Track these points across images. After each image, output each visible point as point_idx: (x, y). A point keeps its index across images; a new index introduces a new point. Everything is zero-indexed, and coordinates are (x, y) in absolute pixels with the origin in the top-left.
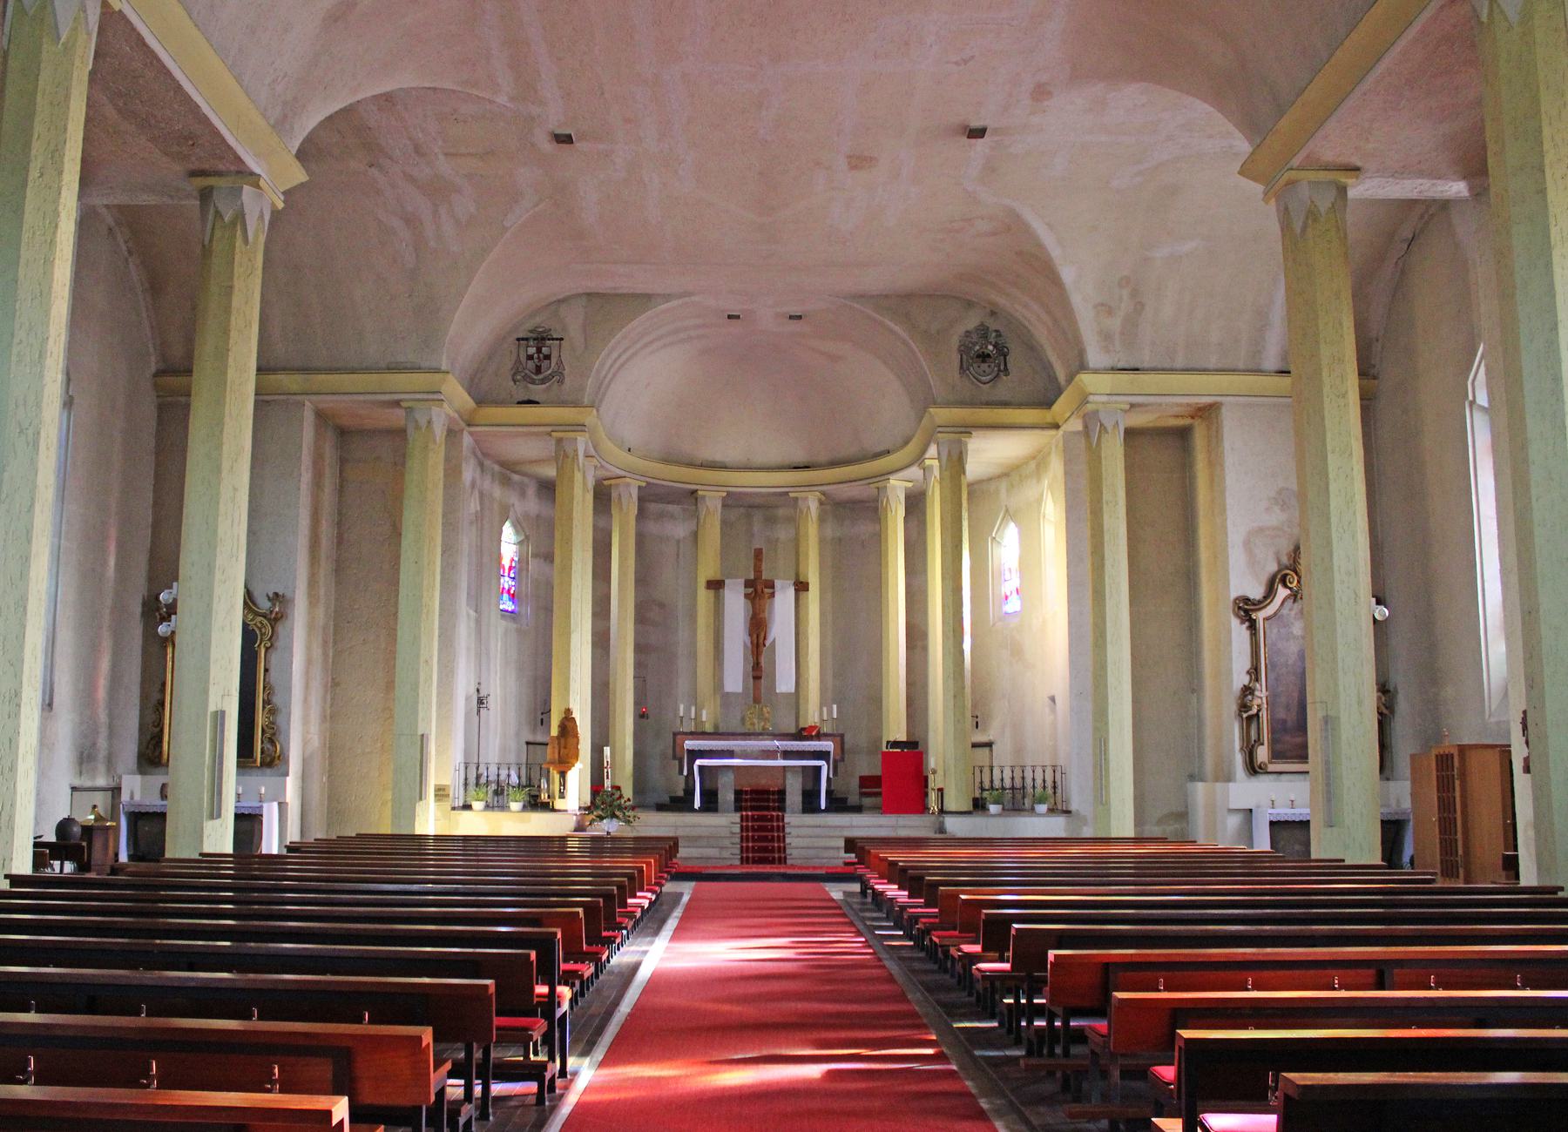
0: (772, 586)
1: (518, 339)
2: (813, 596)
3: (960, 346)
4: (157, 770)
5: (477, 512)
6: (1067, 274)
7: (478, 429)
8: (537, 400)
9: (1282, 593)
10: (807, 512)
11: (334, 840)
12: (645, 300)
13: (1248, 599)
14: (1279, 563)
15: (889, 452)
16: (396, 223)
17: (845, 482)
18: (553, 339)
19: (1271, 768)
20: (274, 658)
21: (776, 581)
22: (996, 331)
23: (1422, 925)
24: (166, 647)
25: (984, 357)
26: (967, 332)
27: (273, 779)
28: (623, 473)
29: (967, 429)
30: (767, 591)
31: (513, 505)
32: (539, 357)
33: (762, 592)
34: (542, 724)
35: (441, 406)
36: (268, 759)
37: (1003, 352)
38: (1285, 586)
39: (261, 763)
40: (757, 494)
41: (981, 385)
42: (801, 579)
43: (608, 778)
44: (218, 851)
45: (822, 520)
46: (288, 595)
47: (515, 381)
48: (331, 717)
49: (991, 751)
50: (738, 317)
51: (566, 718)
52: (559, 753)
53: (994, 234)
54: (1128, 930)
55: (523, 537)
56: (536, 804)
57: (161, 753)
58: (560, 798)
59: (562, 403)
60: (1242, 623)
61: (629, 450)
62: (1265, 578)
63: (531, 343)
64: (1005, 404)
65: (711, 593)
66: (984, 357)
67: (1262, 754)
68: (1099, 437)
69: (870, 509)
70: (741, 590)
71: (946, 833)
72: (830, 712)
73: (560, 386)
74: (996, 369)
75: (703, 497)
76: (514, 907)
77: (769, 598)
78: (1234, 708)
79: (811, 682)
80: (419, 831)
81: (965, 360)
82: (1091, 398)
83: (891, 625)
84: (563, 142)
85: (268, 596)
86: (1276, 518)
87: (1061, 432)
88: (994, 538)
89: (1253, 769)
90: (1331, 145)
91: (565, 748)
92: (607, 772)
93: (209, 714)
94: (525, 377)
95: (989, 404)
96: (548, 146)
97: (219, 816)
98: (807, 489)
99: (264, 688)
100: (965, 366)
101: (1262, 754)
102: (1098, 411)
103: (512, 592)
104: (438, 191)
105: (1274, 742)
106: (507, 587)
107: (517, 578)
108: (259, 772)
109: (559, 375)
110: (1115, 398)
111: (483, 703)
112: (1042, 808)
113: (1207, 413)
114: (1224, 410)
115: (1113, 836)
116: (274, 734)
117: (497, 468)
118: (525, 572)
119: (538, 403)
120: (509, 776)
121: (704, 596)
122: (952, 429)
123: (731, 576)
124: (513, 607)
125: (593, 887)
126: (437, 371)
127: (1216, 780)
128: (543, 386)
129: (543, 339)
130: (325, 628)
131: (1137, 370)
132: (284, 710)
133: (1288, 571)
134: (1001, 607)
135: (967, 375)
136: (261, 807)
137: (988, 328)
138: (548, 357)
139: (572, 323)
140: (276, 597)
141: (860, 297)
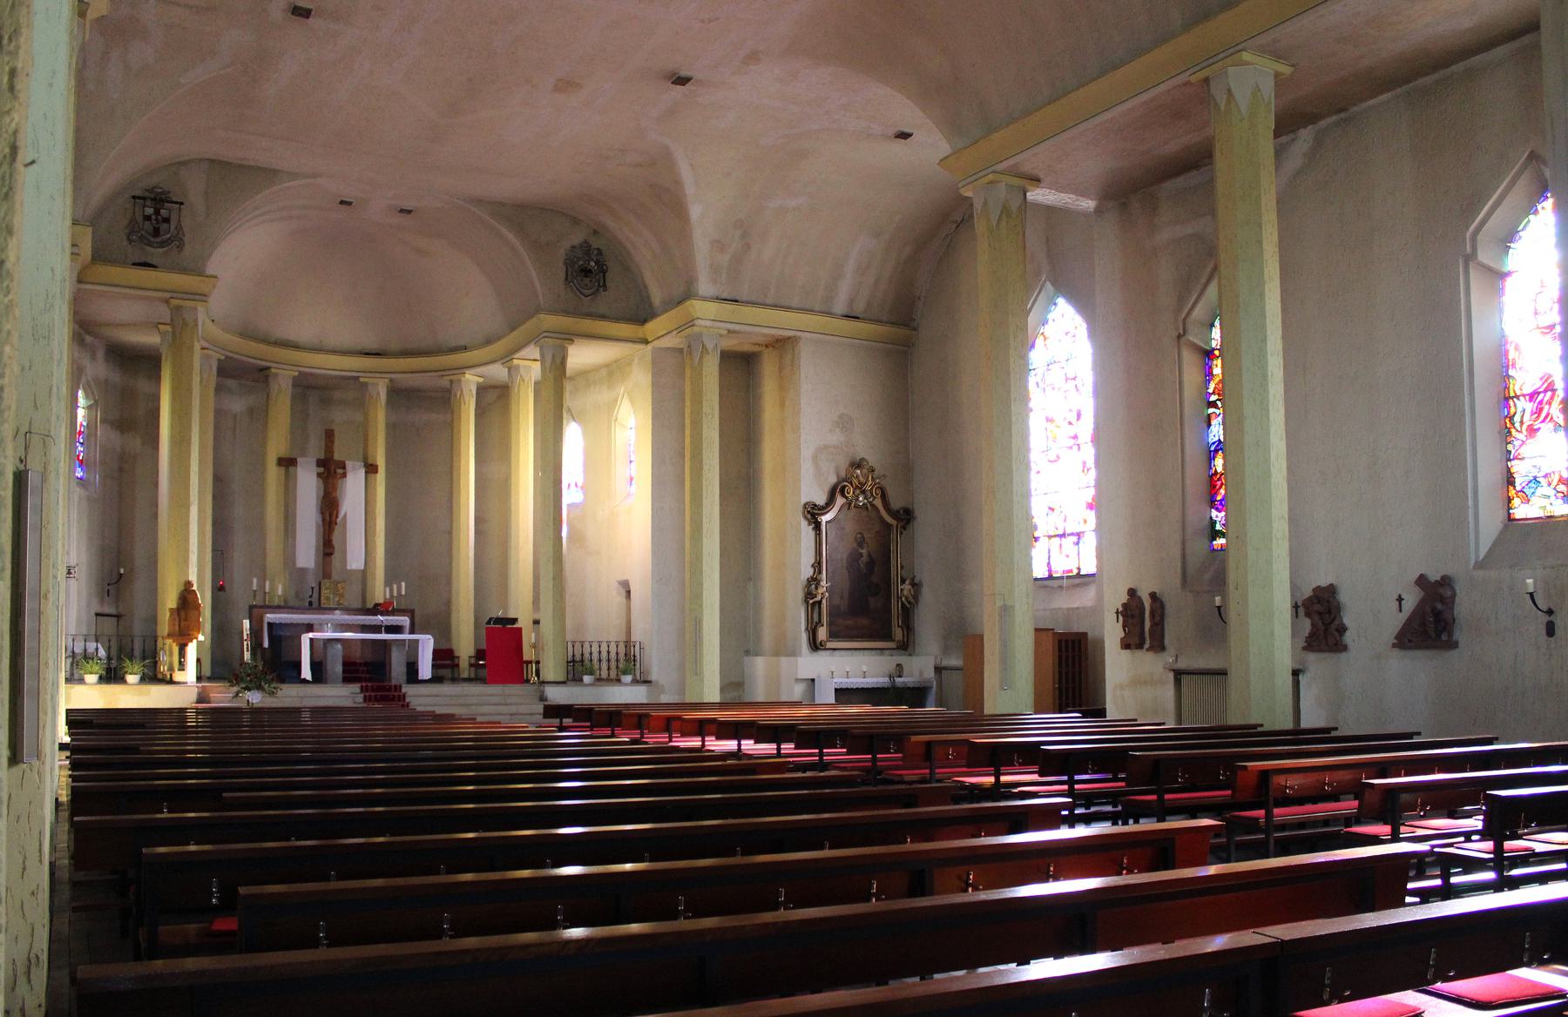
0: (344, 467)
1: (134, 197)
2: (381, 477)
3: (566, 260)
6: (695, 211)
7: (89, 287)
8: (154, 263)
9: (840, 501)
12: (269, 175)
13: (815, 505)
14: (838, 475)
15: (466, 349)
17: (418, 372)
18: (173, 202)
19: (829, 645)
21: (347, 462)
22: (599, 249)
25: (586, 272)
26: (573, 247)
29: (570, 336)
30: (340, 471)
33: (335, 472)
34: (108, 595)
38: (843, 495)
41: (583, 297)
42: (370, 461)
47: (130, 241)
50: (350, 204)
51: (186, 590)
52: (180, 625)
53: (639, 165)
55: (92, 402)
56: (153, 676)
58: (179, 670)
59: (183, 270)
60: (809, 524)
62: (827, 488)
63: (148, 203)
64: (603, 317)
65: (283, 470)
66: (586, 272)
67: (822, 633)
68: (701, 358)
69: (445, 399)
71: (546, 700)
72: (391, 591)
73: (179, 252)
75: (276, 375)
76: (1190, 732)
77: (341, 478)
78: (800, 595)
79: (378, 560)
81: (569, 273)
82: (698, 322)
83: (463, 510)
84: (301, 15)
86: (836, 438)
87: (649, 347)
89: (815, 646)
90: (1031, 161)
91: (186, 620)
92: (247, 645)
94: (141, 238)
98: (378, 375)
100: (569, 279)
101: (822, 633)
105: (830, 624)
107: (85, 443)
109: (177, 241)
110: (717, 324)
111: (71, 573)
112: (628, 678)
113: (782, 344)
114: (801, 344)
115: (705, 701)
118: (93, 439)
119: (156, 267)
120: (97, 649)
121: (273, 473)
123: (303, 455)
124: (82, 474)
127: (777, 653)
128: (161, 250)
129: (162, 201)
131: (736, 301)
133: (846, 483)
137: (591, 246)
138: (167, 220)
139: (194, 189)
141: (479, 201)
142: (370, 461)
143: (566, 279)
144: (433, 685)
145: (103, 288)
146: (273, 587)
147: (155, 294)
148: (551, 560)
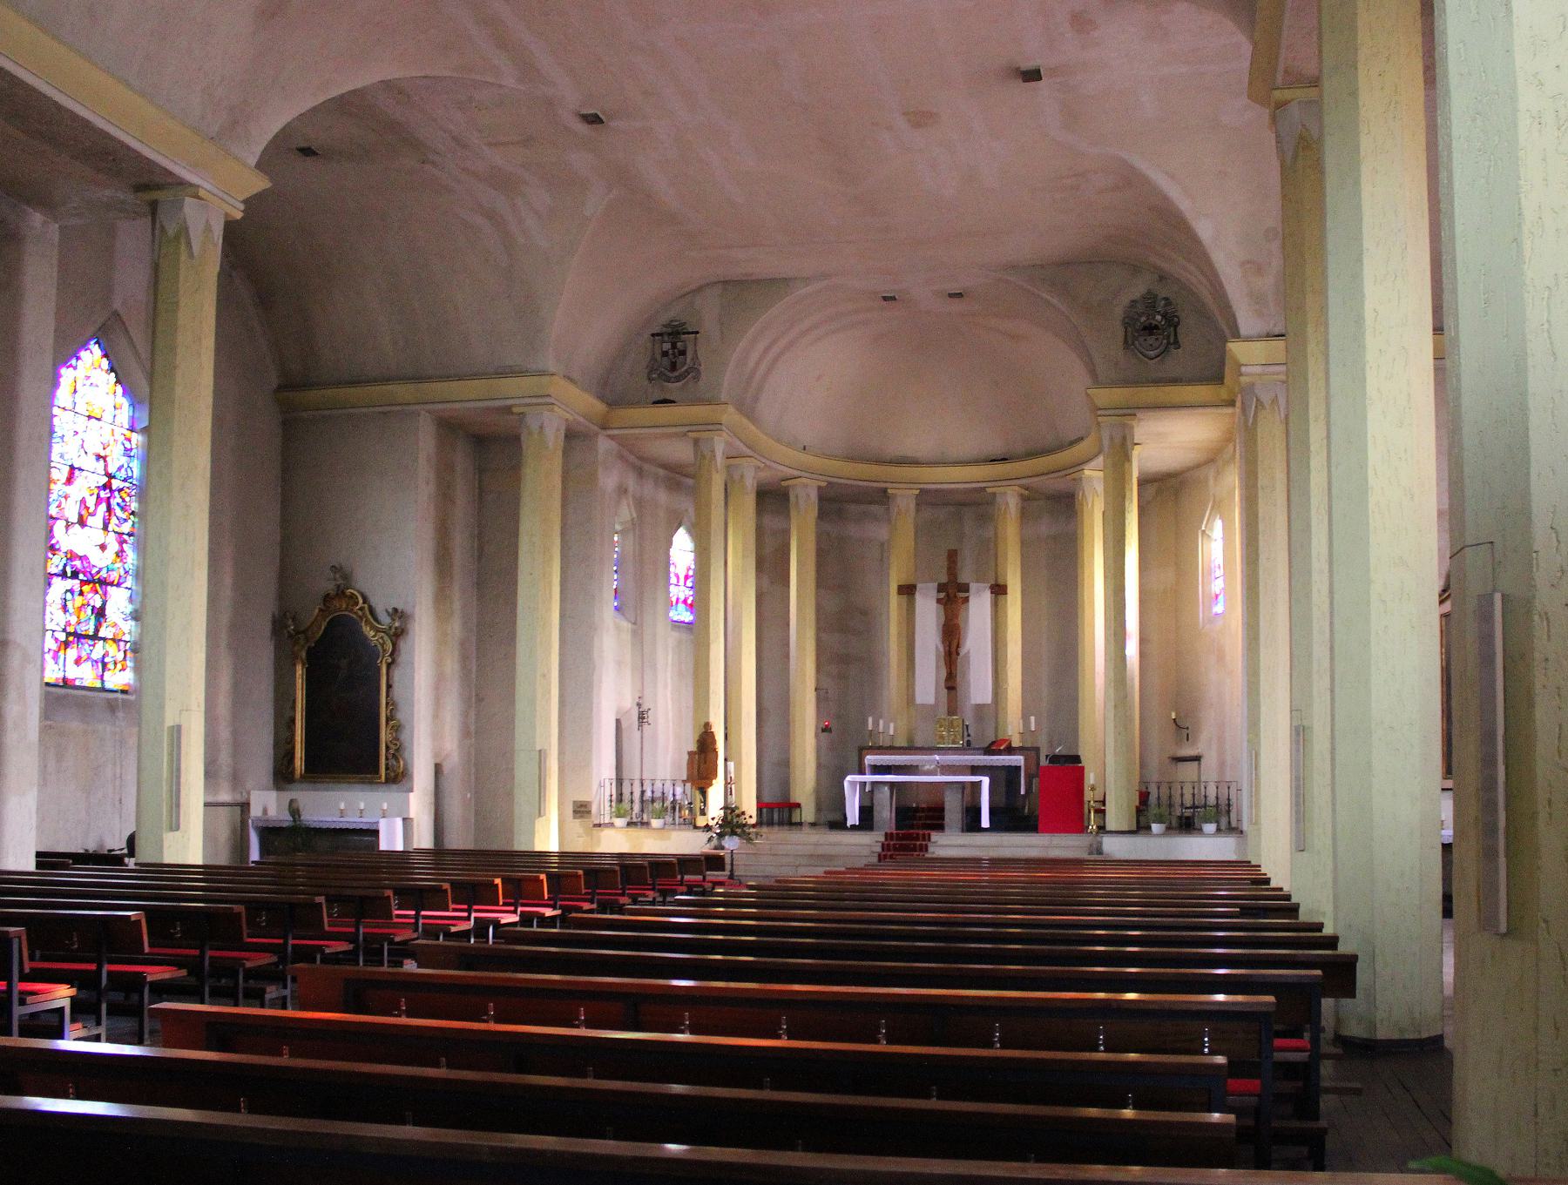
1: (653, 335)
3: (1124, 318)
4: (290, 786)
5: (633, 519)
6: (1204, 230)
10: (1005, 509)
11: (862, 869)
12: (774, 286)
16: (479, 220)
18: (689, 333)
20: (397, 674)
22: (1166, 299)
23: (581, 929)
24: (295, 665)
25: (1150, 329)
26: (1133, 301)
27: (396, 795)
28: (796, 473)
29: (1130, 411)
31: (687, 510)
32: (674, 354)
34: (1188, 740)
35: (552, 410)
36: (392, 774)
37: (1172, 321)
39: (386, 778)
40: (957, 490)
43: (731, 794)
44: (180, 862)
45: (1025, 515)
46: (408, 610)
47: (650, 380)
48: (476, 733)
49: (1199, 764)
50: (893, 298)
54: (1285, 955)
57: (294, 768)
61: (804, 449)
64: (1175, 381)
68: (1256, 413)
69: (1065, 504)
70: (933, 593)
72: (876, 723)
74: (1165, 341)
80: (539, 847)
81: (1129, 334)
82: (1243, 369)
85: (387, 611)
88: (1204, 531)
93: (166, 729)
94: (661, 375)
95: (1157, 382)
96: (583, 128)
97: (178, 828)
98: (1004, 483)
99: (387, 704)
100: (1130, 342)
102: (1253, 384)
103: (689, 602)
104: (503, 182)
106: (682, 598)
108: (384, 787)
109: (693, 371)
110: (1272, 369)
111: (644, 718)
112: (1210, 828)
116: (397, 750)
117: (661, 472)
119: (674, 402)
121: (894, 600)
122: (1117, 412)
125: (696, 909)
126: (542, 373)
128: (680, 383)
129: (678, 333)
130: (462, 644)
132: (407, 727)
134: (1211, 608)
135: (1133, 350)
136: (378, 823)
138: (683, 353)
139: (708, 313)
140: (396, 613)
141: (1013, 267)
142: (1001, 582)
143: (1126, 341)
144: (993, 834)
145: (646, 430)
146: (887, 727)
147: (674, 430)
148: (1112, 684)
